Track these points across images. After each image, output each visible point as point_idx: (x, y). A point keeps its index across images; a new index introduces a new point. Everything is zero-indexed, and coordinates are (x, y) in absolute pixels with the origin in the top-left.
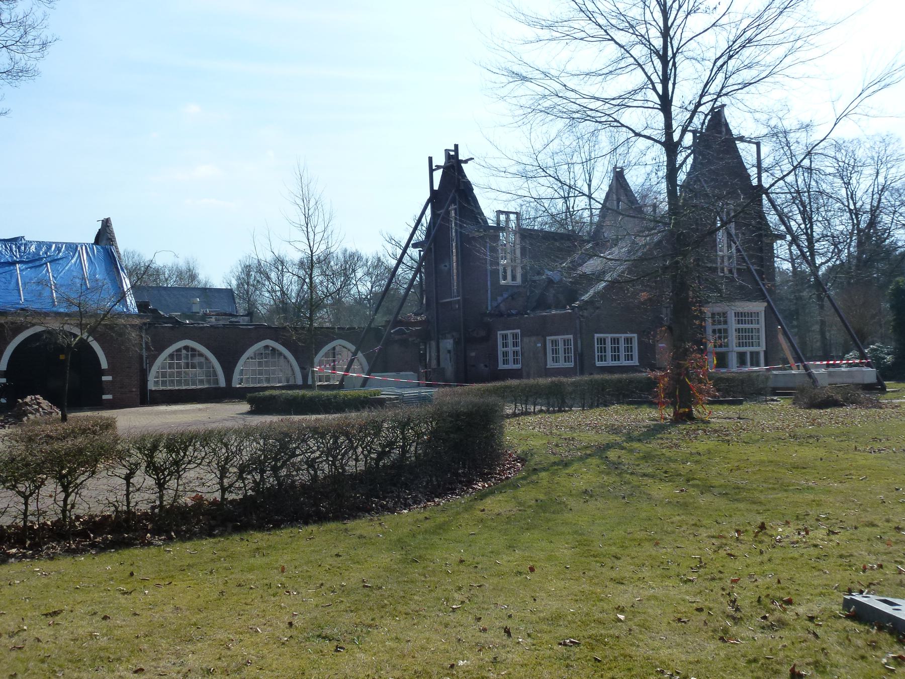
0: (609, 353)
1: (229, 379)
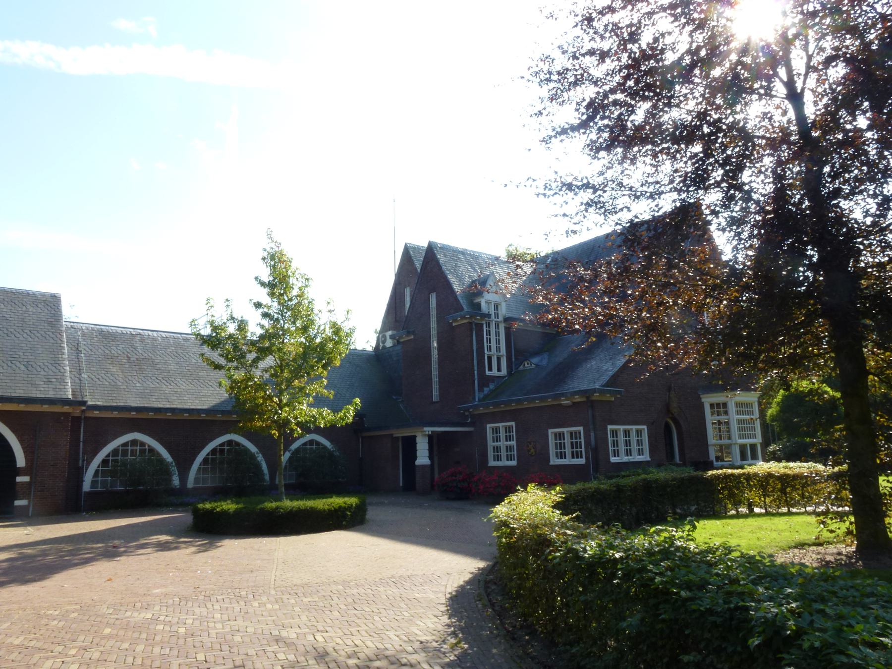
0: (567, 440)
1: (183, 478)
